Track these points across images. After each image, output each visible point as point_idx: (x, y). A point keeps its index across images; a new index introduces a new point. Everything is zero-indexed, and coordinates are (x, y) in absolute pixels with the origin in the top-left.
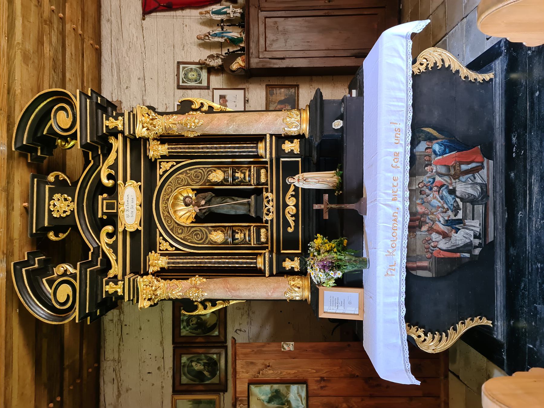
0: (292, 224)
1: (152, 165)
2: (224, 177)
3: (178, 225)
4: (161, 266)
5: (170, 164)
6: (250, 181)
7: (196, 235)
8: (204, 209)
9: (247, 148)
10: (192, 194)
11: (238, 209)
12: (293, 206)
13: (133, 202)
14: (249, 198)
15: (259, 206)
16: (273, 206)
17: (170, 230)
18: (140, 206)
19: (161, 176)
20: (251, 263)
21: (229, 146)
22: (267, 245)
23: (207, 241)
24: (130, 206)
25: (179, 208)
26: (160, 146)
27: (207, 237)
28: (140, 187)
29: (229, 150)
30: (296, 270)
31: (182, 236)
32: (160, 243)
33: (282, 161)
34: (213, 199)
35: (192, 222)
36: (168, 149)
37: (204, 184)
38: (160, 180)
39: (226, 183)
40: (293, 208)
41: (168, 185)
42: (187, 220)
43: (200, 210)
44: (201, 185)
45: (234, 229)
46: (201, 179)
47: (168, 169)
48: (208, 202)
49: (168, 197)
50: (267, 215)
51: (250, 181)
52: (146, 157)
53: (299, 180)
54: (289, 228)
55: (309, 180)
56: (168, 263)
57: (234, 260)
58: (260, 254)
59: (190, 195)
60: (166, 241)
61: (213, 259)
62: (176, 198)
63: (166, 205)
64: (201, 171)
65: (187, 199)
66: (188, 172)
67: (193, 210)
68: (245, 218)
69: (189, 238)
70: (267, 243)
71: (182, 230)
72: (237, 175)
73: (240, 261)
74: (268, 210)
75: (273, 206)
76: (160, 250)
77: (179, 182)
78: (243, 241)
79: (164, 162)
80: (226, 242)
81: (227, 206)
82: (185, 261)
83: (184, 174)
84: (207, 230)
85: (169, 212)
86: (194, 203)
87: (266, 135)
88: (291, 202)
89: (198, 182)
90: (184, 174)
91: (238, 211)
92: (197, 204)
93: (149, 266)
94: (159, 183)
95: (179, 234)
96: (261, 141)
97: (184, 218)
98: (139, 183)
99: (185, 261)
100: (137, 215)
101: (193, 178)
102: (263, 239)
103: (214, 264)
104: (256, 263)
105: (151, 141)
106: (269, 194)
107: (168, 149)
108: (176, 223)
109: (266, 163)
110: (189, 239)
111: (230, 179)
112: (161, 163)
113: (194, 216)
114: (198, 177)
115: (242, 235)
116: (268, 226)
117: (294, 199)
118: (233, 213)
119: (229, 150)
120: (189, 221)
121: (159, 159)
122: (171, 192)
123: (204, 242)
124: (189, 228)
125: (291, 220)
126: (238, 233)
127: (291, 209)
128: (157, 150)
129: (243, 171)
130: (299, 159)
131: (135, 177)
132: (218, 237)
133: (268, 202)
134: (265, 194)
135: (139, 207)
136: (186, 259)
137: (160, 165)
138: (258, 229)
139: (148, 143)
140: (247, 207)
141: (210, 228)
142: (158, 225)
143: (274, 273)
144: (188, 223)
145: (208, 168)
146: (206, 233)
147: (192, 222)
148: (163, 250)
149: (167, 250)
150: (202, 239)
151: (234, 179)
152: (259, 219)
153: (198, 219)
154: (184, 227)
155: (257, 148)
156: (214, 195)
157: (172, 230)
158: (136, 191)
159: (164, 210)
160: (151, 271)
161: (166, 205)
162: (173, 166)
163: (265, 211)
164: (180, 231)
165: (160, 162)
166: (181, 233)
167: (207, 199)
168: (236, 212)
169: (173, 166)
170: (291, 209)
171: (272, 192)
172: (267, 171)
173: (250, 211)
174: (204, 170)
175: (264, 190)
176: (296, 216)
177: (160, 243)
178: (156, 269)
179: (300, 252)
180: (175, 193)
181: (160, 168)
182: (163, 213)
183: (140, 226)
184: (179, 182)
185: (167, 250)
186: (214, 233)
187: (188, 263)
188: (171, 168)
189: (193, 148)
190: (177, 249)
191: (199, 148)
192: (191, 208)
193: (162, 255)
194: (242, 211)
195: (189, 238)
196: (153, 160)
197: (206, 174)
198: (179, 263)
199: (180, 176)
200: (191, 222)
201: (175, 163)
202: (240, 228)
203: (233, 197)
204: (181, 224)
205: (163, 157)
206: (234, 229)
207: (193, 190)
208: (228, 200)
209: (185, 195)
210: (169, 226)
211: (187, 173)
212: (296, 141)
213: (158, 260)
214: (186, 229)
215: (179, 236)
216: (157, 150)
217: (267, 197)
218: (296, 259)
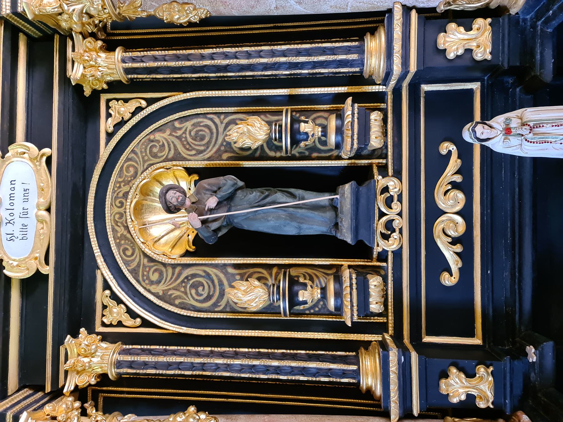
0: (454, 263)
1: (85, 105)
2: (269, 134)
3: (151, 260)
4: (100, 371)
5: (132, 106)
6: (338, 146)
7: (195, 286)
8: (215, 220)
9: (333, 51)
10: (186, 183)
11: (302, 220)
12: (457, 213)
13: (26, 200)
14: (333, 190)
15: (363, 214)
16: (400, 214)
17: (130, 272)
18: (48, 210)
19: (110, 136)
20: (344, 374)
21: (284, 47)
22: (381, 320)
23: (223, 303)
24: (18, 209)
25: (152, 218)
26: (103, 55)
27: (222, 294)
28: (49, 161)
29: (283, 59)
30: (482, 405)
31: (159, 289)
32: (105, 307)
33: (427, 93)
34: (239, 194)
35: (187, 254)
36: (123, 61)
37: (218, 156)
38: (107, 144)
39: (272, 154)
40: (459, 219)
41: (128, 159)
42: (173, 247)
43: (204, 222)
44: (209, 159)
45: (294, 272)
46: (209, 142)
47: (126, 118)
48: (227, 201)
49: (125, 189)
50: (386, 237)
51: (338, 146)
52: (65, 79)
53: (508, 131)
54: (446, 275)
55: (547, 129)
56: (119, 364)
57: (294, 364)
58: (367, 344)
59: (184, 185)
60: (119, 301)
61: (236, 355)
62: (145, 192)
63: (121, 210)
64: (210, 123)
65: (171, 194)
66: (177, 124)
67: (187, 223)
68: (325, 245)
69: (177, 293)
70: (384, 314)
71: (161, 274)
72: (304, 127)
73: (313, 365)
74: (389, 225)
75: (400, 214)
76: (104, 325)
77: (155, 150)
78: (315, 305)
79: (118, 100)
80: (270, 309)
81: (277, 213)
82: (162, 359)
83: (168, 132)
84: (222, 276)
85: (127, 228)
86: (188, 203)
87: (390, 11)
88: (450, 202)
89: (201, 152)
90: (168, 132)
91: (304, 226)
92: (197, 207)
93: (66, 372)
94: (104, 152)
95: (152, 283)
96: (373, 32)
97: (166, 244)
98: (47, 150)
99: (162, 359)
100: (37, 235)
101: (189, 140)
102: (375, 307)
103: (240, 371)
104: (356, 374)
105: (78, 38)
106: (392, 183)
107: (123, 61)
108: (145, 255)
109: (380, 97)
110: (176, 297)
111: (286, 141)
112: (111, 104)
113: (191, 238)
114: (202, 138)
115: (318, 294)
116: (386, 269)
117: (461, 196)
118: (291, 230)
119: (283, 59)
120: (180, 250)
121: (104, 91)
122: (135, 176)
123: (215, 305)
124: (178, 270)
125: (450, 254)
126: (305, 285)
127: (451, 224)
128: (92, 65)
129: (319, 121)
130: (475, 86)
131: (38, 136)
132: (251, 295)
133: (389, 202)
134: (381, 181)
135: (45, 213)
136: (165, 353)
137: (108, 107)
138: (362, 274)
139: (70, 43)
140: (330, 214)
141: (231, 270)
142: (100, 261)
143: (416, 412)
144: (175, 256)
145: (227, 114)
146: (221, 283)
147: (187, 254)
148: (111, 325)
149: (120, 324)
150: (209, 297)
151: (295, 142)
152: (361, 250)
153: (201, 248)
154: (164, 265)
155: (361, 50)
156: (241, 183)
157: (134, 272)
158: (37, 172)
159: (116, 222)
160: (69, 387)
161: (121, 210)
162: (139, 109)
163: (380, 226)
164: (155, 277)
165: (108, 101)
166: (158, 282)
167: (221, 194)
168: (300, 228)
169: (139, 109)
170: (451, 224)
171: (398, 174)
172: (385, 120)
173: (336, 225)
174: (217, 120)
175: (375, 170)
176: (465, 240)
177: (105, 307)
178: (83, 381)
179: (477, 341)
180: (140, 181)
181: (109, 115)
182: (113, 230)
183: (47, 262)
184: (155, 150)
185: (120, 324)
186: (242, 285)
187: (169, 366)
188: (134, 114)
189: (187, 58)
190: (146, 323)
191: (203, 57)
192: (181, 217)
193: (105, 337)
194: (316, 226)
195: (177, 293)
196: (87, 92)
197: (221, 129)
198: (145, 365)
199: (158, 136)
200: (182, 251)
201: (144, 103)
202: (309, 271)
203: (292, 190)
204: (155, 257)
205: (114, 86)
206: (294, 272)
207: (190, 171)
208: (279, 196)
209: (168, 181)
210: (126, 263)
211: (175, 129)
212: (479, 22)
213: (93, 355)
214: (170, 270)
215: (153, 288)
216: (92, 65)
217: (386, 189)
218: (481, 370)
